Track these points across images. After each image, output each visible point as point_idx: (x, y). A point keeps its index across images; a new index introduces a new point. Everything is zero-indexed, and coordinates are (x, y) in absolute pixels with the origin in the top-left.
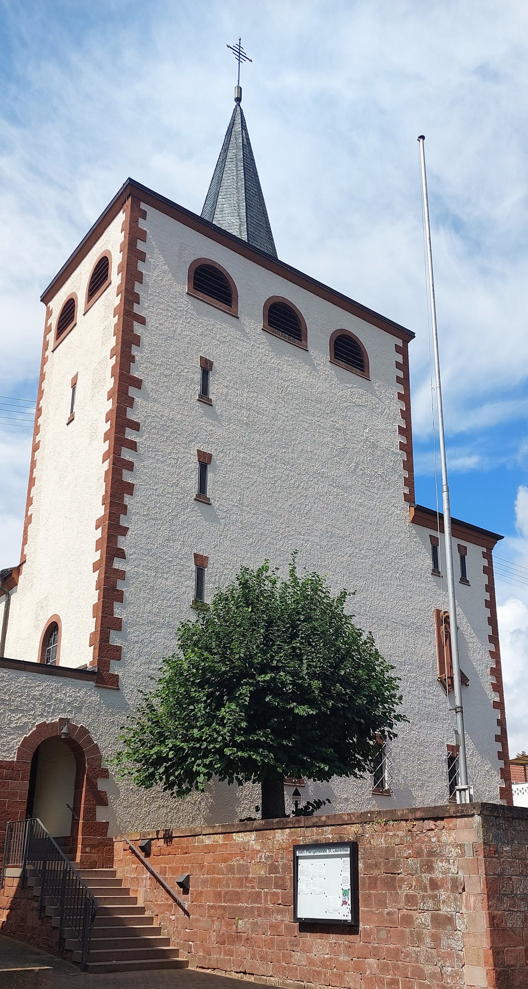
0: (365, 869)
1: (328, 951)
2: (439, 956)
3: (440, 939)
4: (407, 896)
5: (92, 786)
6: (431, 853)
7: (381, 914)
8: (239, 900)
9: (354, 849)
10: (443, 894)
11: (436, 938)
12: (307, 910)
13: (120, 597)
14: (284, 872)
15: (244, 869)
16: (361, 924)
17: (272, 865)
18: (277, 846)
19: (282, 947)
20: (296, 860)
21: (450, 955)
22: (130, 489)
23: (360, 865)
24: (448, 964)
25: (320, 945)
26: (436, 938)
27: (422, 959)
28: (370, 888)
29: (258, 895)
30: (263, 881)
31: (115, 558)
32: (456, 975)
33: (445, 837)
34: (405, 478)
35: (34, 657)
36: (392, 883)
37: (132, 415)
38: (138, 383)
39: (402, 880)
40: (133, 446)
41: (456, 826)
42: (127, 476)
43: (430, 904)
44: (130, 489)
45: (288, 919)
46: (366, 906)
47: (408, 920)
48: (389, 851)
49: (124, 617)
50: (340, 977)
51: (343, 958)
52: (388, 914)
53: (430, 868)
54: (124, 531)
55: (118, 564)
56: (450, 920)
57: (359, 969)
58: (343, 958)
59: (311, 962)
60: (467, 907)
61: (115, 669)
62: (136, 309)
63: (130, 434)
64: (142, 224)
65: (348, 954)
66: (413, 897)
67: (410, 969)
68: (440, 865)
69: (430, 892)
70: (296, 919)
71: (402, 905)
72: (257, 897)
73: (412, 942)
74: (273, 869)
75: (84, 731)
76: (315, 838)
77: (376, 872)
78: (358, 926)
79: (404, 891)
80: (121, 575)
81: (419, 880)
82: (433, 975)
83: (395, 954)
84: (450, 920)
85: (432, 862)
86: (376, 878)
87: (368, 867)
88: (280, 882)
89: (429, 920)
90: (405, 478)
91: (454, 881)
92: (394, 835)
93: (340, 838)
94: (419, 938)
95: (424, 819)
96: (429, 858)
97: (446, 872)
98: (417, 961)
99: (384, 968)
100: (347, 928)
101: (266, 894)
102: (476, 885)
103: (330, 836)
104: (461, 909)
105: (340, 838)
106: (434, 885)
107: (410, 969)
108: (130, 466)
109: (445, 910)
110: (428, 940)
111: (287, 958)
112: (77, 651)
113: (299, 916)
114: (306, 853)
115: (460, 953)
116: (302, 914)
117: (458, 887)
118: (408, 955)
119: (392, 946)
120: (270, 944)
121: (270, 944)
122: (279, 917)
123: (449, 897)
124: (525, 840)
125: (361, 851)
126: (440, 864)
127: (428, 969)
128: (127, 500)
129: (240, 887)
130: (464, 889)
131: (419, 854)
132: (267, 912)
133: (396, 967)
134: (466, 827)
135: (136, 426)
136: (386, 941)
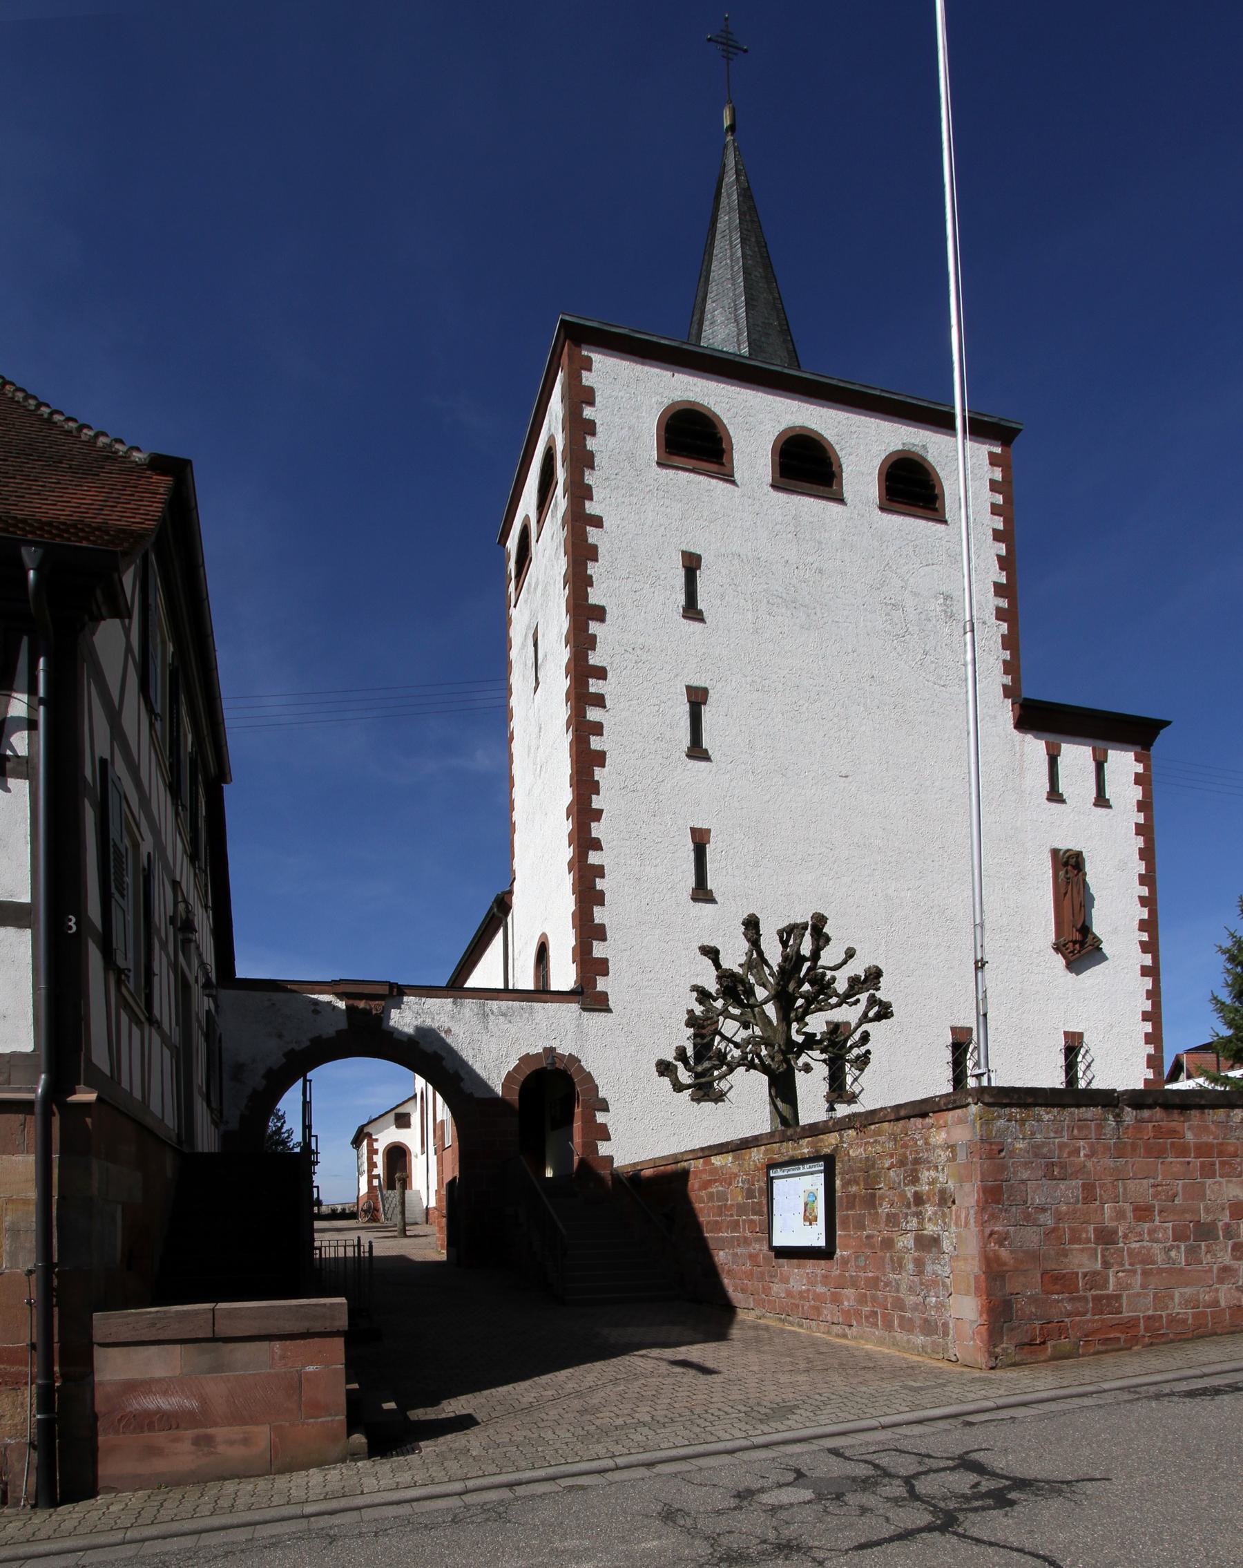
0: (843, 1186)
1: (805, 1281)
2: (922, 1284)
3: (924, 1264)
4: (888, 1214)
5: (590, 1119)
6: (917, 1161)
7: (860, 1237)
8: (720, 1230)
9: (830, 1164)
10: (929, 1210)
11: (919, 1264)
12: (781, 1238)
13: (599, 898)
14: (760, 1196)
15: (722, 1197)
16: (838, 1251)
17: (749, 1189)
18: (752, 1167)
19: (761, 1277)
20: (770, 1181)
21: (934, 1283)
22: (600, 758)
23: (838, 1183)
24: (932, 1293)
25: (798, 1276)
26: (919, 1264)
27: (903, 1287)
28: (848, 1209)
29: (737, 1222)
30: (742, 1209)
31: (591, 853)
32: (940, 1306)
33: (939, 1137)
34: (998, 556)
35: (530, 986)
36: (871, 1201)
37: (594, 659)
38: (599, 614)
39: (882, 1198)
40: (599, 701)
41: (946, 1122)
42: (596, 743)
43: (914, 1223)
44: (600, 758)
45: (765, 1248)
46: (844, 1230)
47: (888, 1244)
48: (869, 1165)
49: (606, 922)
50: (817, 1309)
51: (820, 1289)
52: (868, 1237)
53: (915, 1180)
54: (598, 815)
55: (594, 858)
56: (935, 1241)
57: (836, 1299)
58: (820, 1289)
59: (789, 1294)
60: (956, 1225)
61: (602, 984)
62: (591, 508)
63: (595, 686)
64: (588, 379)
65: (825, 1284)
66: (895, 1215)
67: (890, 1300)
68: (925, 1175)
69: (914, 1209)
70: (771, 1248)
71: (883, 1225)
72: (735, 1226)
73: (894, 1269)
74: (750, 1194)
75: (573, 1059)
76: (791, 1153)
77: (854, 1189)
78: (834, 1253)
79: (884, 1209)
80: (599, 871)
81: (903, 1195)
82: (915, 1308)
83: (874, 1283)
84: (935, 1241)
85: (916, 1171)
86: (855, 1196)
87: (846, 1184)
88: (757, 1207)
89: (912, 1242)
90: (998, 556)
91: (943, 1192)
92: (876, 1141)
93: (817, 1151)
94: (899, 1266)
95: (909, 1118)
96: (912, 1167)
97: (933, 1182)
98: (898, 1291)
99: (862, 1300)
100: (824, 1254)
101: (744, 1221)
102: (968, 1197)
103: (806, 1151)
104: (949, 1226)
105: (817, 1151)
106: (919, 1199)
107: (890, 1300)
108: (598, 729)
109: (930, 1229)
110: (911, 1266)
111: (767, 1291)
112: (563, 976)
113: (775, 1244)
114: (779, 1173)
115: (946, 1280)
116: (778, 1241)
117: (945, 1199)
118: (887, 1284)
119: (870, 1275)
120: (750, 1276)
121: (750, 1276)
122: (757, 1247)
123: (935, 1213)
124: (701, 1209)
125: (838, 1166)
126: (927, 1174)
127: (911, 1300)
128: (598, 773)
129: (720, 1215)
130: (954, 1202)
131: (902, 1163)
132: (746, 1241)
133: (874, 1298)
134: (961, 1121)
135: (601, 673)
136: (864, 1269)
